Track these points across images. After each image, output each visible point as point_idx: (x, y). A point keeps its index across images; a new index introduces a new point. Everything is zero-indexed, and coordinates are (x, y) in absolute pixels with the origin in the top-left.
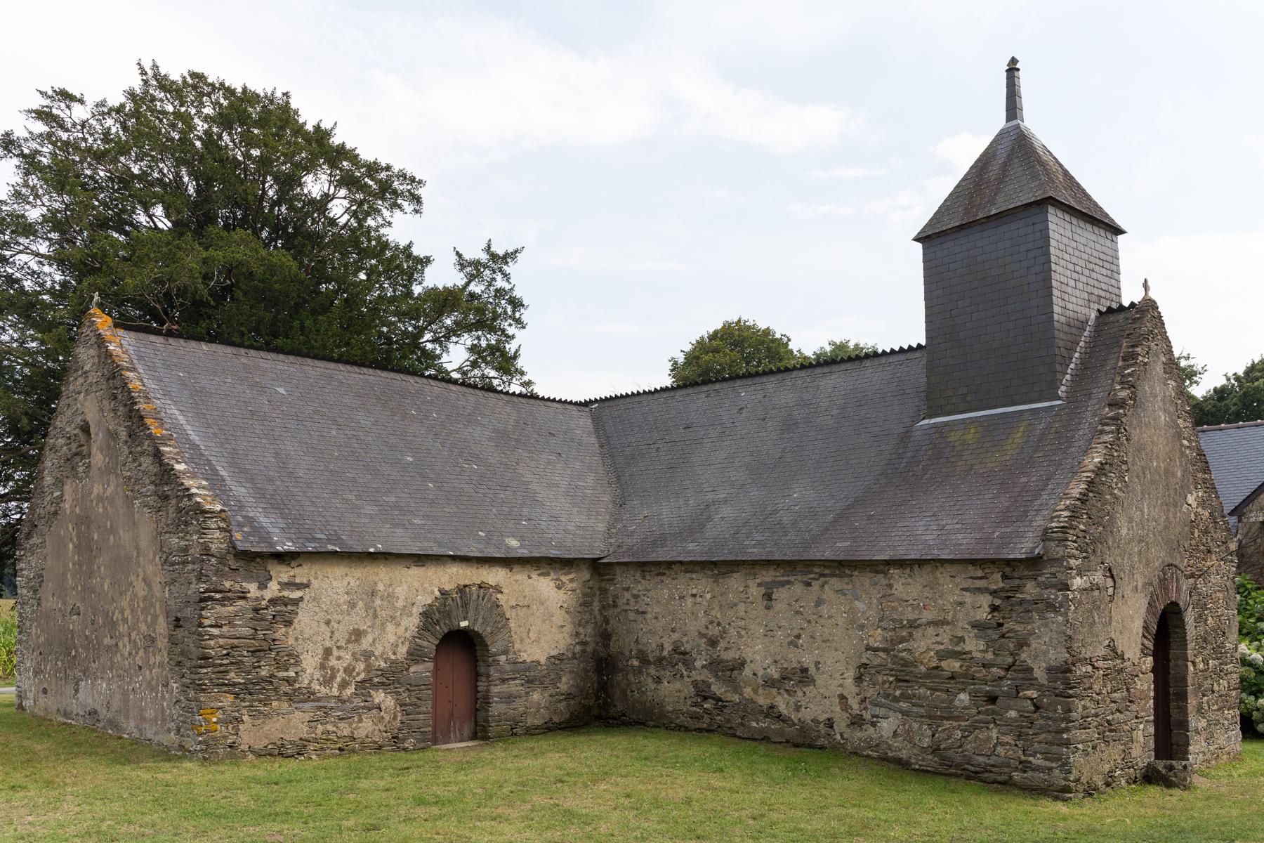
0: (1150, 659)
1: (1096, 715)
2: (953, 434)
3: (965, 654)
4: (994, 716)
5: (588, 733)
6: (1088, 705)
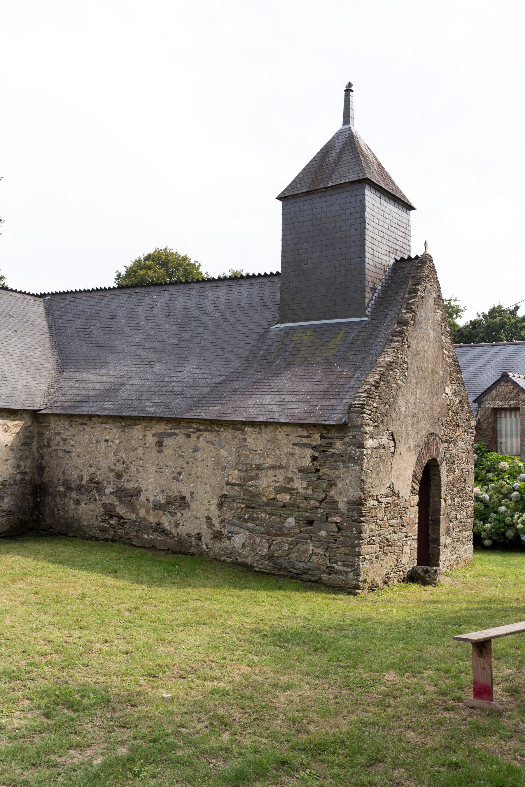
0: (416, 498)
1: (379, 535)
2: (295, 335)
3: (293, 490)
4: (311, 534)
5: (23, 541)
6: (374, 528)
